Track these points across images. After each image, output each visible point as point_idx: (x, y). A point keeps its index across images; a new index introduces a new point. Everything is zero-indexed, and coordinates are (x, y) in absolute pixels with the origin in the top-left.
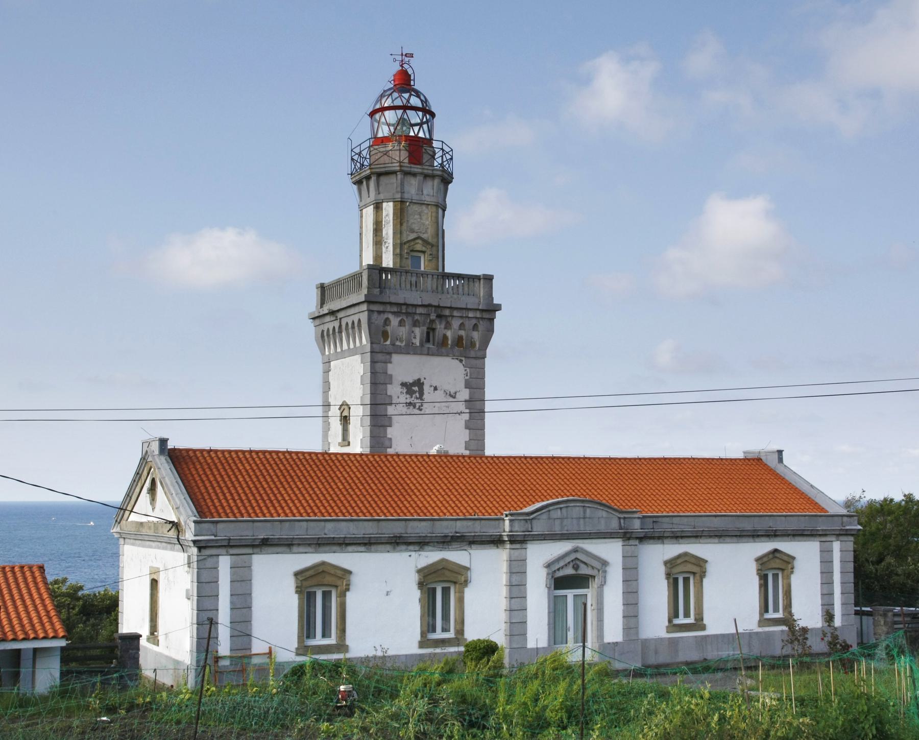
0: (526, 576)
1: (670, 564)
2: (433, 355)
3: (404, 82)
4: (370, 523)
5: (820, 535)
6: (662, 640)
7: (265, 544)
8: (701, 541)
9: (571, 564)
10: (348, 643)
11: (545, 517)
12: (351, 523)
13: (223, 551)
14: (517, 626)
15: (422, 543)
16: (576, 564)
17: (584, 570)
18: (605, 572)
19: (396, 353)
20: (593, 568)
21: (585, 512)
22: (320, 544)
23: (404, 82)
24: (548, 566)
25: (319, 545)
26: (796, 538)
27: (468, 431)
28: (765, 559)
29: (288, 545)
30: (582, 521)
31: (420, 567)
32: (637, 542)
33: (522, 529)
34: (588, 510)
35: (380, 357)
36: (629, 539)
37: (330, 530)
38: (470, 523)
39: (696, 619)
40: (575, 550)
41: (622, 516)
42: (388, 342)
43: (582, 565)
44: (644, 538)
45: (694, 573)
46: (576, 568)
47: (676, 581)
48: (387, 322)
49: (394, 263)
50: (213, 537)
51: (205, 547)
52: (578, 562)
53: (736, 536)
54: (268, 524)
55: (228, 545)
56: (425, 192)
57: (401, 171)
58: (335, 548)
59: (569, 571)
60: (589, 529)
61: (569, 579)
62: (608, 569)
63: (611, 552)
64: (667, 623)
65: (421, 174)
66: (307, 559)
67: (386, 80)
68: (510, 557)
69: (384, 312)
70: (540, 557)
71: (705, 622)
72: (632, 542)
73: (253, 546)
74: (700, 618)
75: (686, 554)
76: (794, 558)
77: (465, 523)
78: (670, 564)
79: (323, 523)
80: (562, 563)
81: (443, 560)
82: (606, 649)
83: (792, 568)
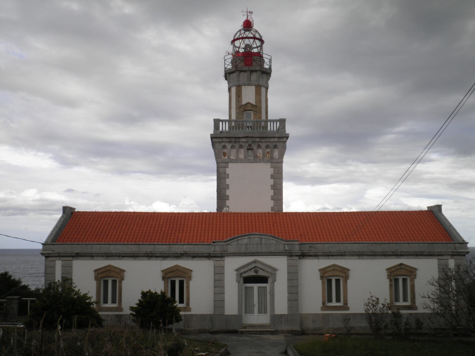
0: (224, 275)
1: (323, 272)
2: (252, 162)
3: (248, 25)
4: (134, 246)
5: (438, 255)
6: (317, 315)
7: (78, 256)
8: (345, 258)
9: (253, 269)
10: (123, 306)
11: (235, 243)
12: (124, 246)
13: (58, 258)
14: (219, 302)
15: (164, 256)
16: (256, 269)
17: (261, 273)
18: (275, 274)
19: (231, 162)
20: (268, 272)
21: (261, 240)
22: (108, 256)
23: (248, 25)
24: (237, 270)
25: (108, 256)
26: (418, 257)
27: (273, 201)
28: (394, 269)
29: (91, 256)
30: (259, 246)
31: (163, 269)
32: (297, 258)
33: (221, 250)
34: (263, 240)
35: (222, 165)
36: (291, 256)
37: (113, 249)
38: (192, 246)
39: (344, 304)
40: (255, 262)
41: (287, 243)
42: (226, 157)
43: (260, 271)
44: (303, 255)
45: (342, 277)
46: (256, 272)
47: (396, 281)
48: (224, 147)
49: (236, 118)
50: (51, 252)
51: (49, 257)
52: (257, 269)
53: (371, 255)
54: (80, 246)
55: (60, 256)
56: (252, 79)
57: (237, 70)
58: (116, 258)
59: (252, 273)
60: (264, 250)
61: (254, 278)
62: (277, 273)
63: (280, 264)
64: (321, 305)
65: (249, 70)
66: (394, 262)
67: (239, 25)
68: (214, 265)
69: (222, 142)
70: (232, 265)
71: (349, 305)
72: (293, 258)
73: (73, 257)
74: (346, 303)
75: (334, 265)
76: (416, 269)
77: (189, 246)
78: (323, 272)
79: (108, 246)
80: (246, 269)
81: (176, 266)
82: (276, 318)
83: (415, 275)
